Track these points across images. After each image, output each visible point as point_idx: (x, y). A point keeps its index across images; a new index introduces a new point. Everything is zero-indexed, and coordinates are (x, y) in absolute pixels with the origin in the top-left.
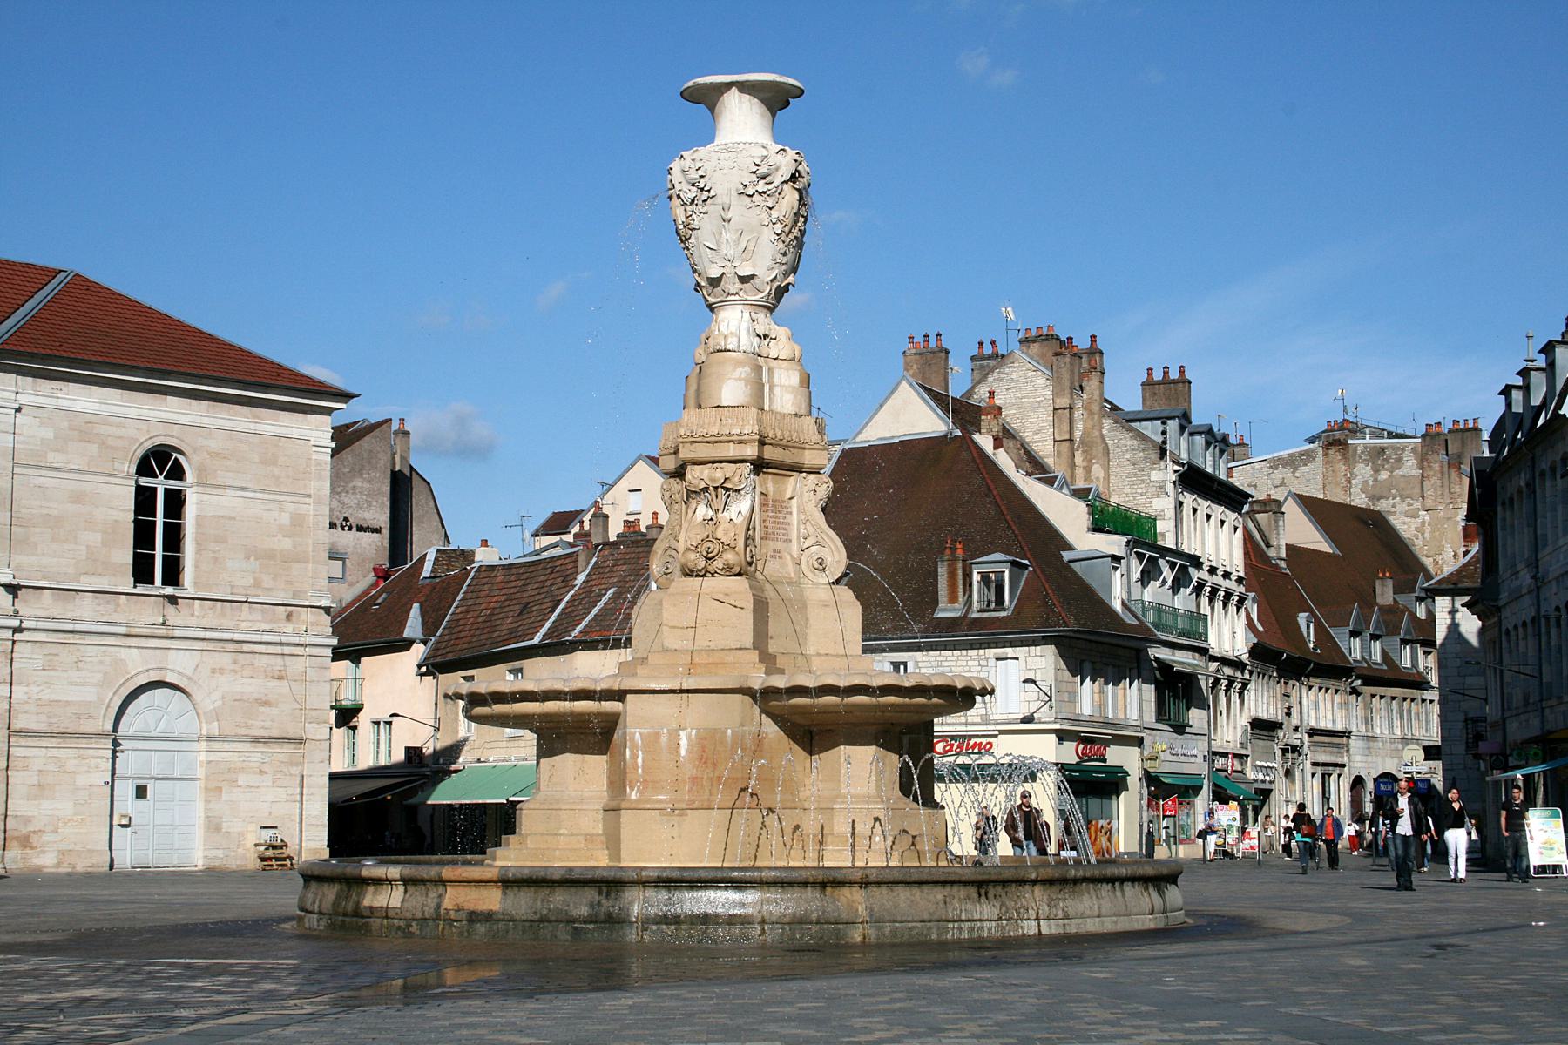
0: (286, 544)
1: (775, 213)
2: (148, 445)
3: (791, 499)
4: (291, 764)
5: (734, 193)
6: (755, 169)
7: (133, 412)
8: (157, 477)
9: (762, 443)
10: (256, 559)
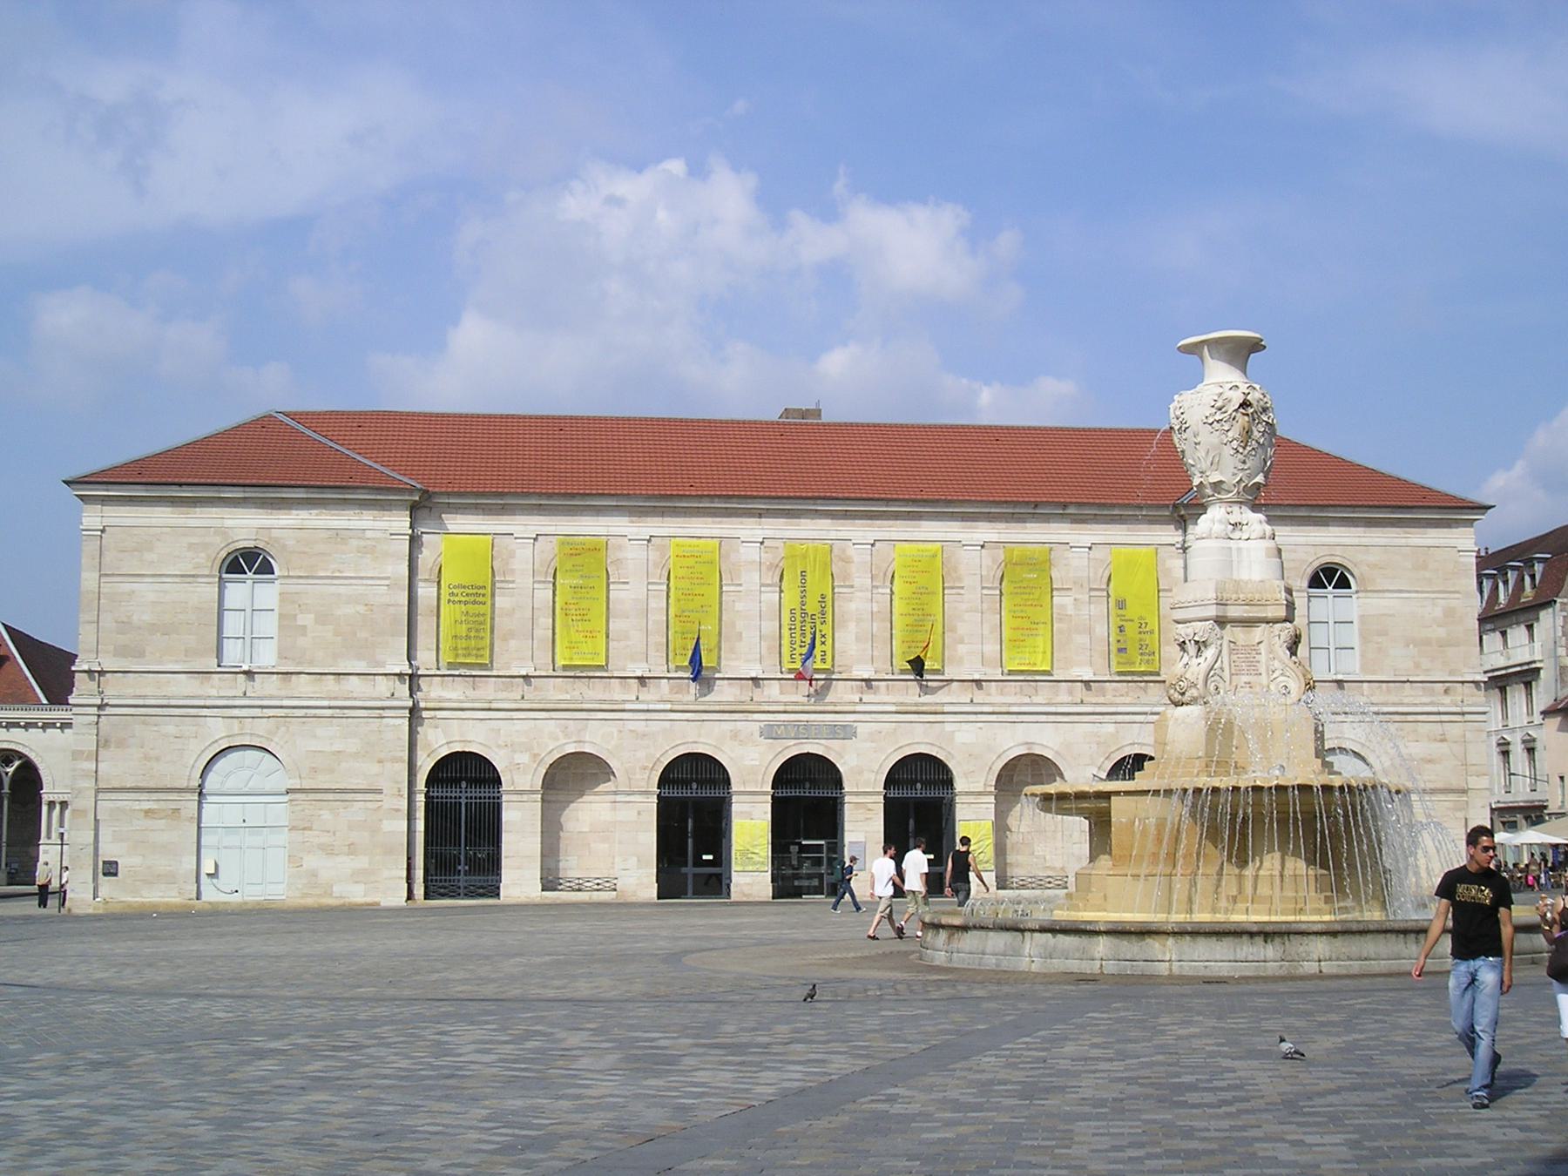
0: (1441, 632)
1: (1230, 434)
2: (1316, 564)
3: (1259, 643)
4: (1456, 809)
5: (1201, 423)
6: (1213, 403)
7: (1302, 540)
8: (1326, 588)
9: (1221, 603)
10: (1415, 646)
